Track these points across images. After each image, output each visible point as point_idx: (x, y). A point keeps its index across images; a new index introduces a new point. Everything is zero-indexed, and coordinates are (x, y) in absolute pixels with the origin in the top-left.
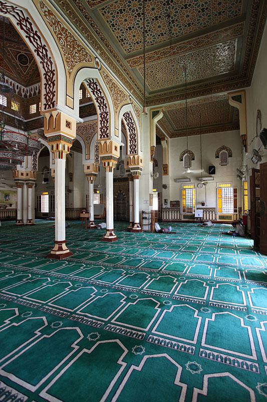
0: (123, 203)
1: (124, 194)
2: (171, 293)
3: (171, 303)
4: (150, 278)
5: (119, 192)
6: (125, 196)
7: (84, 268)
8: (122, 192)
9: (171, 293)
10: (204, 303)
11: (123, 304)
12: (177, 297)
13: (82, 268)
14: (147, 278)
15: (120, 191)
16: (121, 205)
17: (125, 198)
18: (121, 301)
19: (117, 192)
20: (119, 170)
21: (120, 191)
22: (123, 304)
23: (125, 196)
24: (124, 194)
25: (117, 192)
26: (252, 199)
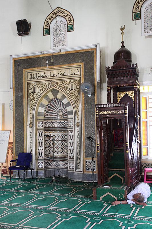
0: (65, 129)
1: (65, 101)
2: (100, 212)
3: (100, 219)
4: (90, 223)
5: (51, 96)
6: (69, 109)
7: (8, 212)
8: (59, 96)
9: (100, 212)
10: (129, 218)
11: (58, 220)
12: (106, 215)
13: (14, 196)
14: (87, 221)
15: (55, 92)
16: (57, 135)
17: (71, 113)
18: (57, 218)
19: (46, 97)
20: (51, 37)
21: (55, 92)
22: (58, 220)
23: (69, 109)
24: (65, 101)
25: (46, 97)
26: (14, 125)
